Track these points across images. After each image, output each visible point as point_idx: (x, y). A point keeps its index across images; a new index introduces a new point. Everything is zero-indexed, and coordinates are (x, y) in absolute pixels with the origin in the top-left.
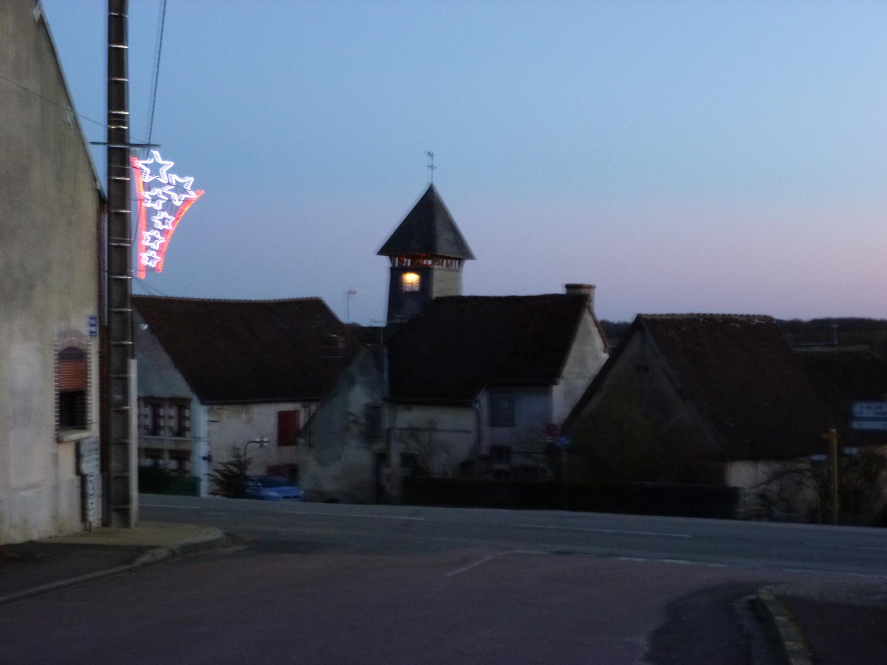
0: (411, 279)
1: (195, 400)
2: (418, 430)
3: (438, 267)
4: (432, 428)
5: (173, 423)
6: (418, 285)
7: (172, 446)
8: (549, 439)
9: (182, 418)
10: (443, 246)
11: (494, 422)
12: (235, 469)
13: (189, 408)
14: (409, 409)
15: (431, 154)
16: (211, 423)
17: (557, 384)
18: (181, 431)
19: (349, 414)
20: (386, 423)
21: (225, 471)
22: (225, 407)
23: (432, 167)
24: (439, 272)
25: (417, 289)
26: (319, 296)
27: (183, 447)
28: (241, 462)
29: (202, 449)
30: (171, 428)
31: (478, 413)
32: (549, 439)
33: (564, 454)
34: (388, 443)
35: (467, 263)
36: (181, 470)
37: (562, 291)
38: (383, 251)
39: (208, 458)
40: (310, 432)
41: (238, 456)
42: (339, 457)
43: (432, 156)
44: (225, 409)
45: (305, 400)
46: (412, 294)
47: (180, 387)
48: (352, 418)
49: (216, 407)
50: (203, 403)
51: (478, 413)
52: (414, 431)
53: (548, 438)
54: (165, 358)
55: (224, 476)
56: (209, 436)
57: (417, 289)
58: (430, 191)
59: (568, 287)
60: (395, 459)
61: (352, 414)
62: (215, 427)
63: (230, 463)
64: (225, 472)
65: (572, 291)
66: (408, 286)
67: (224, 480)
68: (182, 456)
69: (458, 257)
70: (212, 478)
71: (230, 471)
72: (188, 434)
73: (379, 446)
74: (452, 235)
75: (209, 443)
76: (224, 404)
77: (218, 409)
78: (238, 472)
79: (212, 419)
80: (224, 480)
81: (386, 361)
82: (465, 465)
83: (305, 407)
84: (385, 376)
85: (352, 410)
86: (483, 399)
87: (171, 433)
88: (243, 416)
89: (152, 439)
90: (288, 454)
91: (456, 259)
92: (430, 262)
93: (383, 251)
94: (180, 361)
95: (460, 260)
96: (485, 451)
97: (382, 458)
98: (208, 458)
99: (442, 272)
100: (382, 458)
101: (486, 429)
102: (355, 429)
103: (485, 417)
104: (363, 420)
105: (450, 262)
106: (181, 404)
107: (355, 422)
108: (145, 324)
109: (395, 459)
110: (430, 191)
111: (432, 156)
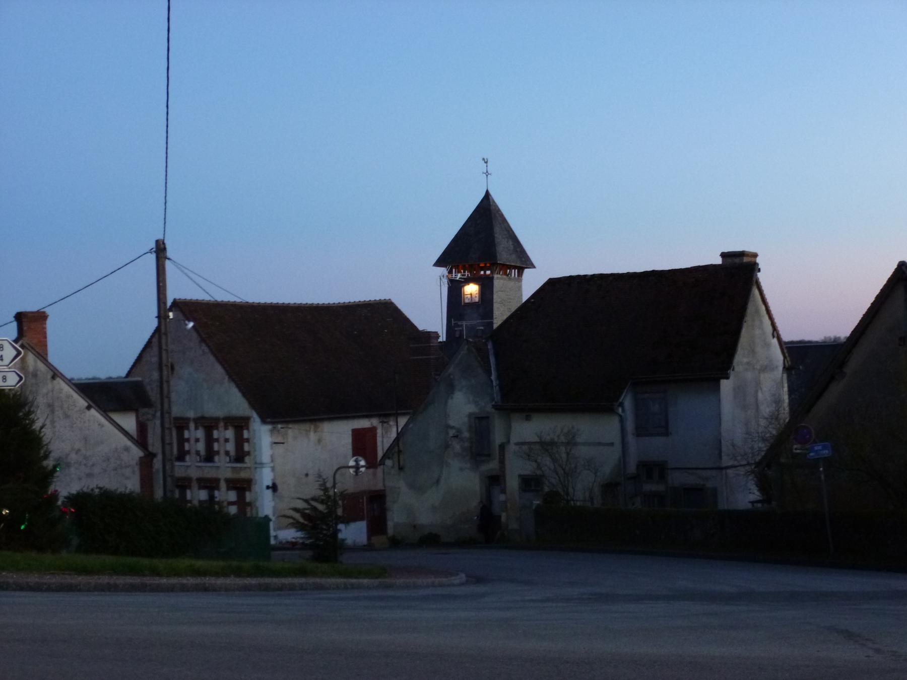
0: (471, 290)
1: (255, 416)
2: (552, 443)
3: (499, 276)
4: (571, 442)
5: (231, 447)
6: (477, 295)
7: (229, 475)
8: (796, 449)
9: (240, 441)
10: (504, 255)
11: (641, 431)
12: (321, 507)
13: (248, 429)
14: (528, 418)
15: (486, 161)
16: (274, 445)
17: (727, 378)
18: (240, 456)
19: (449, 427)
20: (498, 438)
21: (307, 509)
22: (290, 426)
23: (487, 174)
24: (499, 282)
25: (477, 300)
26: (387, 298)
27: (243, 475)
28: (329, 497)
29: (266, 477)
30: (227, 453)
31: (622, 420)
32: (796, 449)
33: (821, 469)
34: (502, 462)
35: (527, 272)
36: (242, 503)
37: (719, 261)
38: (439, 263)
39: (274, 488)
40: (400, 452)
41: (326, 490)
42: (438, 482)
43: (486, 162)
44: (290, 428)
45: (385, 413)
46: (472, 305)
47: (237, 404)
48: (452, 433)
49: (279, 426)
50: (264, 421)
51: (622, 420)
52: (530, 450)
53: (795, 446)
54: (219, 370)
55: (304, 515)
56: (272, 461)
57: (477, 300)
58: (487, 195)
59: (724, 255)
60: (513, 483)
61: (452, 428)
62: (280, 449)
63: (314, 499)
64: (307, 511)
65: (729, 260)
66: (467, 297)
67: (306, 522)
68: (242, 486)
69: (518, 265)
70: (291, 521)
71: (314, 509)
72: (247, 459)
73: (492, 466)
74: (511, 242)
75: (273, 469)
76: (288, 422)
77: (282, 428)
78: (326, 511)
79: (276, 441)
80: (306, 522)
81: (492, 360)
82: (610, 487)
83: (383, 422)
84: (493, 377)
85: (452, 423)
86: (627, 401)
87: (228, 459)
88: (313, 436)
89: (206, 467)
90: (370, 480)
91: (515, 267)
92: (488, 272)
93: (439, 263)
94: (236, 375)
95: (521, 270)
96: (632, 469)
97: (495, 480)
98: (274, 488)
99: (502, 281)
100: (495, 480)
101: (630, 438)
102: (457, 446)
103: (630, 425)
104: (466, 434)
105: (510, 271)
106: (240, 424)
107: (456, 437)
108: (189, 321)
109: (513, 483)
110: (487, 195)
111: (486, 162)
